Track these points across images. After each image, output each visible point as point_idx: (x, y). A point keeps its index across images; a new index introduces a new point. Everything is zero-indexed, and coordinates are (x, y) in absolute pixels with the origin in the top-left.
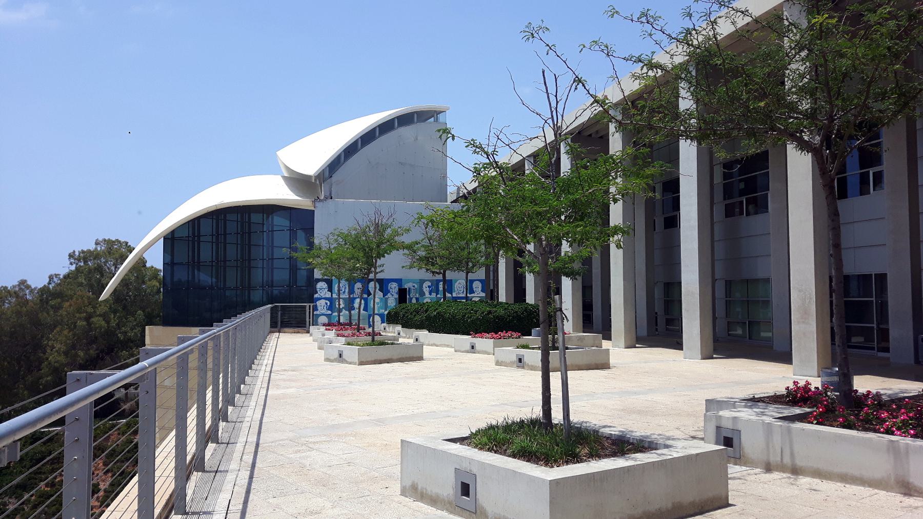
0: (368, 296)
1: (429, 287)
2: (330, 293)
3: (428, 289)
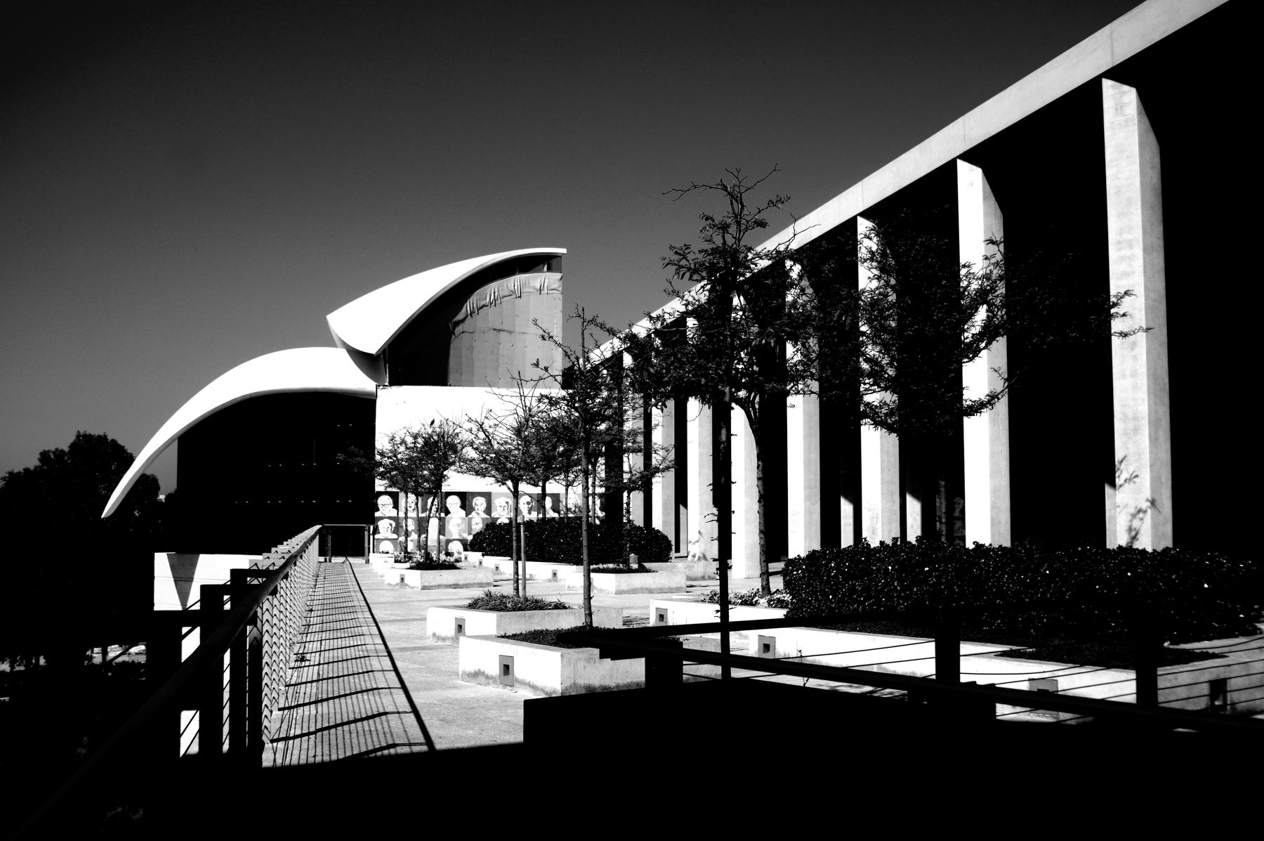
0: (446, 515)
1: (528, 503)
2: (396, 511)
3: (526, 506)
